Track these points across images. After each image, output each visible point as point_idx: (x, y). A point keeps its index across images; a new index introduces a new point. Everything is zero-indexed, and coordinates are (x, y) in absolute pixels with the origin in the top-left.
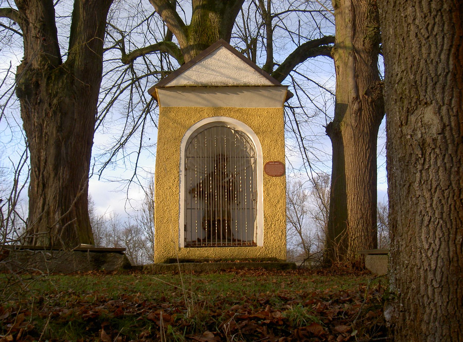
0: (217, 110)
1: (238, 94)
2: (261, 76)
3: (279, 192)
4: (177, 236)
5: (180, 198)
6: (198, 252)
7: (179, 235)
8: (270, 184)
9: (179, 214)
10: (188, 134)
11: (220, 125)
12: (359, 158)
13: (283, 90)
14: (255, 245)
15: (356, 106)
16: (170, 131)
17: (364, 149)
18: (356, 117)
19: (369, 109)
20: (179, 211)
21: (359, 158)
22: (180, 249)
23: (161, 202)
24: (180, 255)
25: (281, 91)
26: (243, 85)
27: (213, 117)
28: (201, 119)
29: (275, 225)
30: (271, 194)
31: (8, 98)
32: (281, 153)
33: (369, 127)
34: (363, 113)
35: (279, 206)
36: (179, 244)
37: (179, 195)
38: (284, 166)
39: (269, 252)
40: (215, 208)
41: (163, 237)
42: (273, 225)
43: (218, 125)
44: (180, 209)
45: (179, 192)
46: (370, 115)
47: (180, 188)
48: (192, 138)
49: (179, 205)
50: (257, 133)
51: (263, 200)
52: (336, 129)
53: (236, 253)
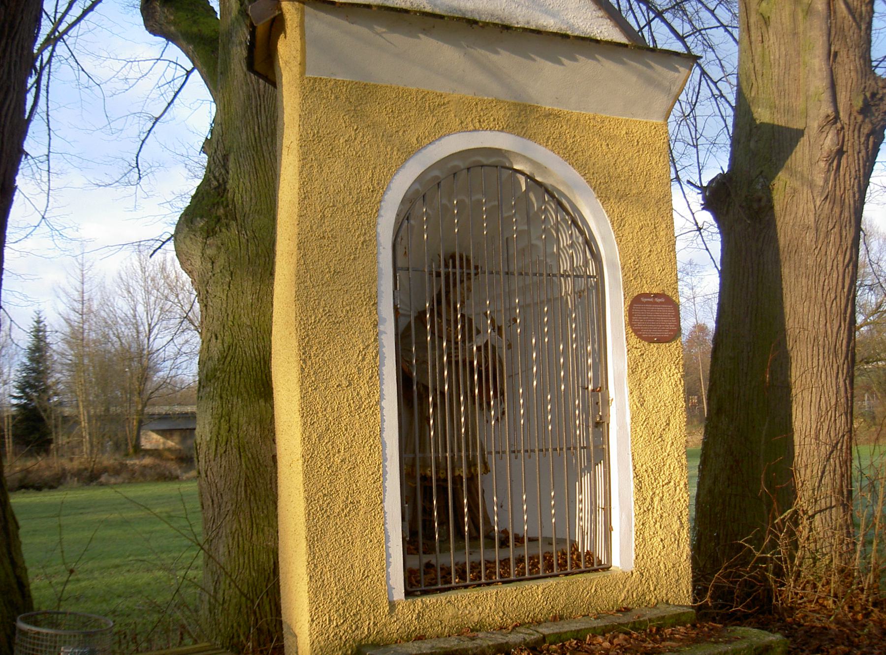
0: (523, 116)
1: (560, 63)
2: (600, 13)
3: (669, 392)
4: (381, 559)
5: (383, 421)
6: (450, 611)
7: (389, 556)
8: (645, 366)
9: (385, 480)
10: (403, 182)
11: (492, 160)
12: (826, 288)
13: (682, 69)
14: (591, 564)
15: (829, 142)
16: (338, 166)
17: (841, 265)
18: (828, 171)
19: (859, 152)
20: (384, 467)
21: (826, 288)
22: (392, 605)
23: (320, 437)
24: (395, 627)
25: (677, 70)
26: (534, 27)
27: (475, 130)
28: (439, 133)
29: (661, 500)
30: (649, 399)
31: (70, 13)
32: (668, 267)
33: (855, 201)
34: (844, 161)
35: (669, 437)
36: (390, 590)
37: (382, 409)
38: (676, 307)
39: (648, 588)
40: (460, 450)
41: (333, 569)
42: (656, 499)
43: (484, 161)
44: (385, 460)
45: (382, 397)
46: (859, 170)
47: (382, 384)
48: (410, 201)
49: (384, 444)
50: (604, 199)
51: (629, 421)
52: (760, 200)
53: (562, 600)
